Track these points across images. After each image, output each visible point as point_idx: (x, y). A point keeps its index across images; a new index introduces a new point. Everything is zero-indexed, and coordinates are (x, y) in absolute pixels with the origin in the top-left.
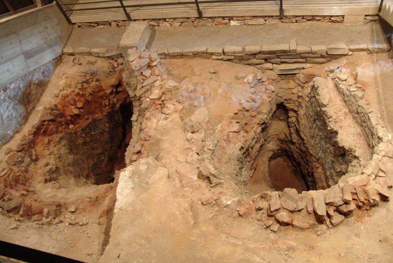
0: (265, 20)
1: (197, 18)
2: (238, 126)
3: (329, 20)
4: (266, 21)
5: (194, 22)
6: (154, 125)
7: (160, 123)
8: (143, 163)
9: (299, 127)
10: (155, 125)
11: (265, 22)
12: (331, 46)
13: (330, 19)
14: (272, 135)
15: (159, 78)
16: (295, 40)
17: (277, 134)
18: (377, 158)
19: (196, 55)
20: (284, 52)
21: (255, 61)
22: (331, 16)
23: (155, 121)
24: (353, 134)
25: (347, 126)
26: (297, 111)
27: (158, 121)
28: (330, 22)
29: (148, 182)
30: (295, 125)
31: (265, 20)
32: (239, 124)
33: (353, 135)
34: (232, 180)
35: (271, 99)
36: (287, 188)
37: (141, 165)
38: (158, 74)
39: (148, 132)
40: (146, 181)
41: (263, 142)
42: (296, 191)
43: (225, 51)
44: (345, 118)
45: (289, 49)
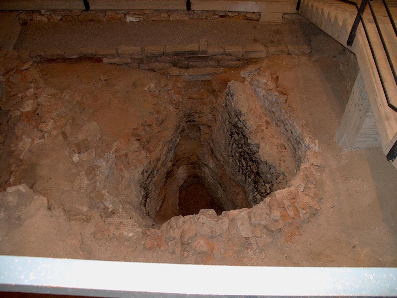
0: (169, 15)
1: (83, 10)
2: (139, 144)
3: (243, 17)
4: (171, 16)
5: (80, 17)
6: (28, 146)
7: (36, 142)
8: (12, 192)
9: (214, 147)
10: (29, 145)
11: (169, 18)
12: (248, 49)
13: (245, 16)
14: (182, 159)
15: (32, 85)
16: (206, 39)
17: (188, 157)
18: (305, 167)
19: (82, 59)
20: (194, 52)
21: (157, 65)
22: (247, 13)
23: (28, 141)
24: (277, 145)
25: (270, 137)
26: (211, 127)
27: (33, 140)
28: (245, 19)
29: (20, 216)
30: (209, 144)
31: (169, 15)
32: (139, 142)
33: (276, 147)
34: (134, 211)
35: (178, 110)
36: (203, 209)
37: (8, 195)
38: (31, 80)
39: (19, 155)
40: (17, 216)
41: (170, 167)
42: (214, 211)
43: (119, 52)
44: (267, 128)
45: (198, 50)
